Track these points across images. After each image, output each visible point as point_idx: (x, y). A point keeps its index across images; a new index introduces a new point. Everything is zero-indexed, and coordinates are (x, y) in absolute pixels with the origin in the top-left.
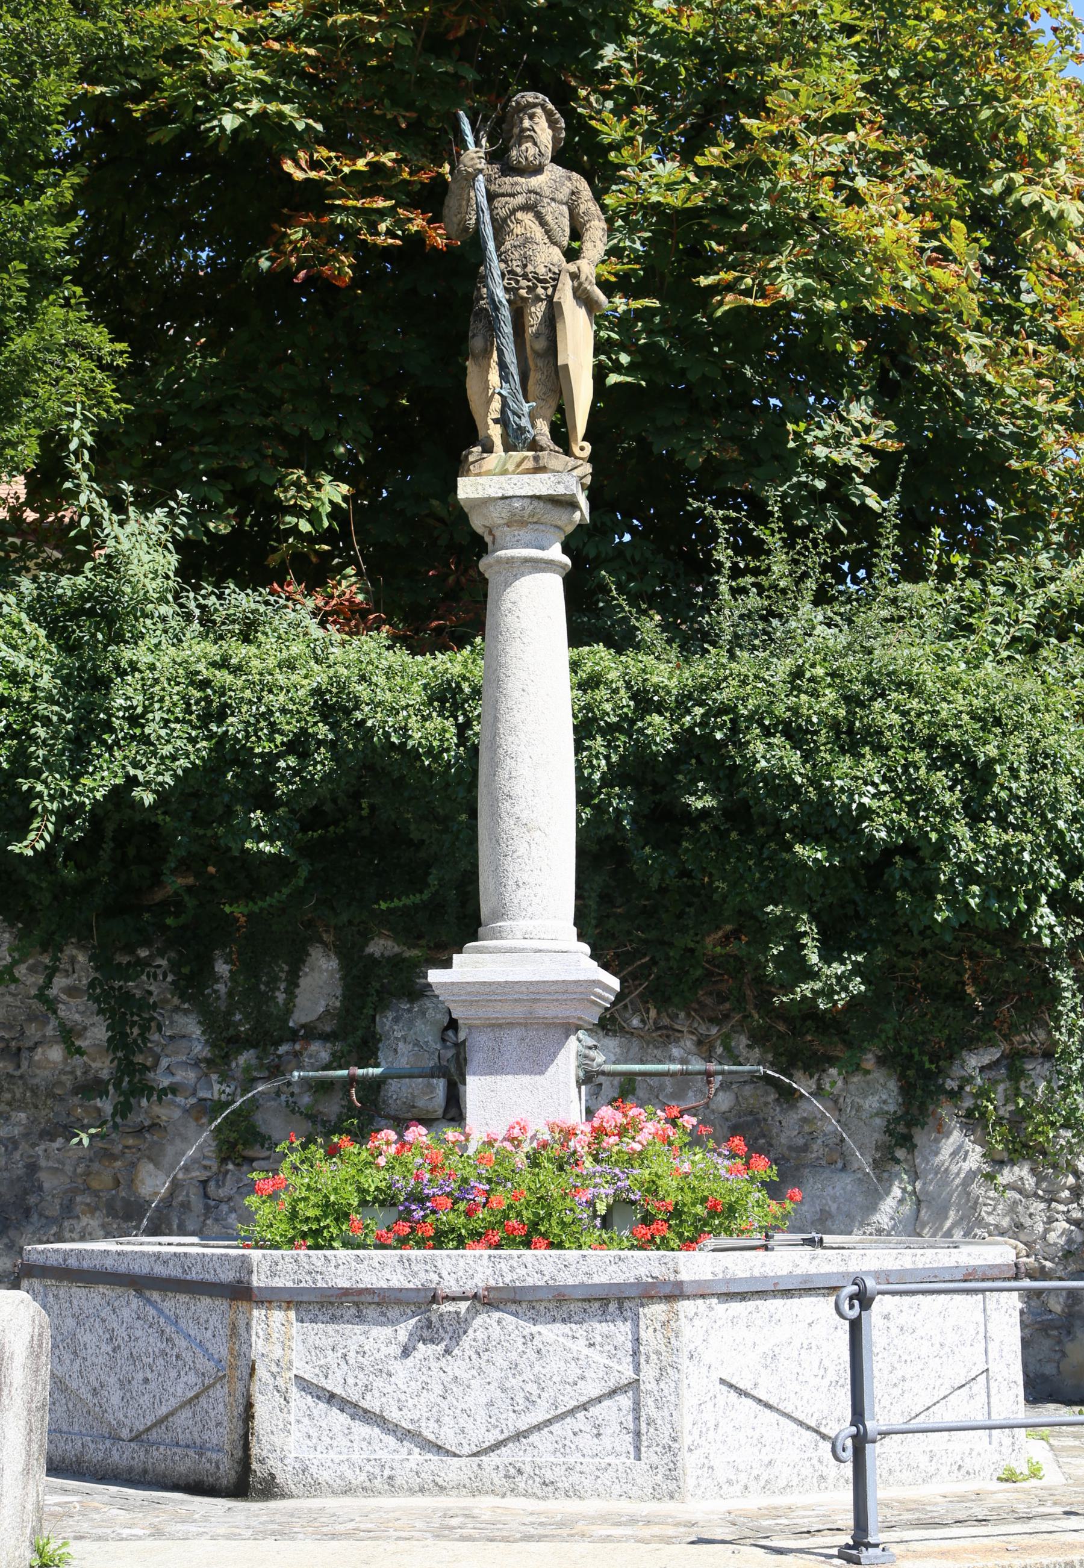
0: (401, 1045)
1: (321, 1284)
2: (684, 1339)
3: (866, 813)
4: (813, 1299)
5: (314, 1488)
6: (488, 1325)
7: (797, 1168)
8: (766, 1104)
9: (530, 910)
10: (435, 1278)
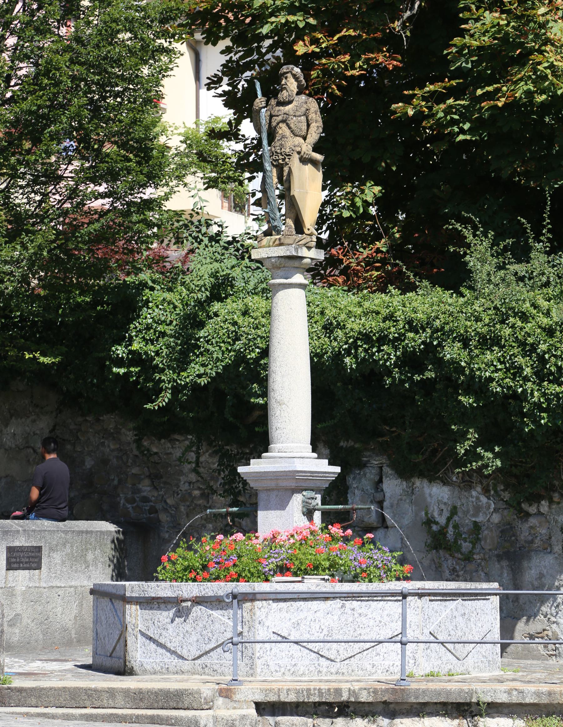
0: (356, 491)
1: (147, 595)
2: (257, 616)
3: (491, 379)
4: (318, 602)
5: (145, 672)
6: (198, 611)
7: (529, 552)
8: (514, 519)
9: (281, 439)
10: (180, 592)
